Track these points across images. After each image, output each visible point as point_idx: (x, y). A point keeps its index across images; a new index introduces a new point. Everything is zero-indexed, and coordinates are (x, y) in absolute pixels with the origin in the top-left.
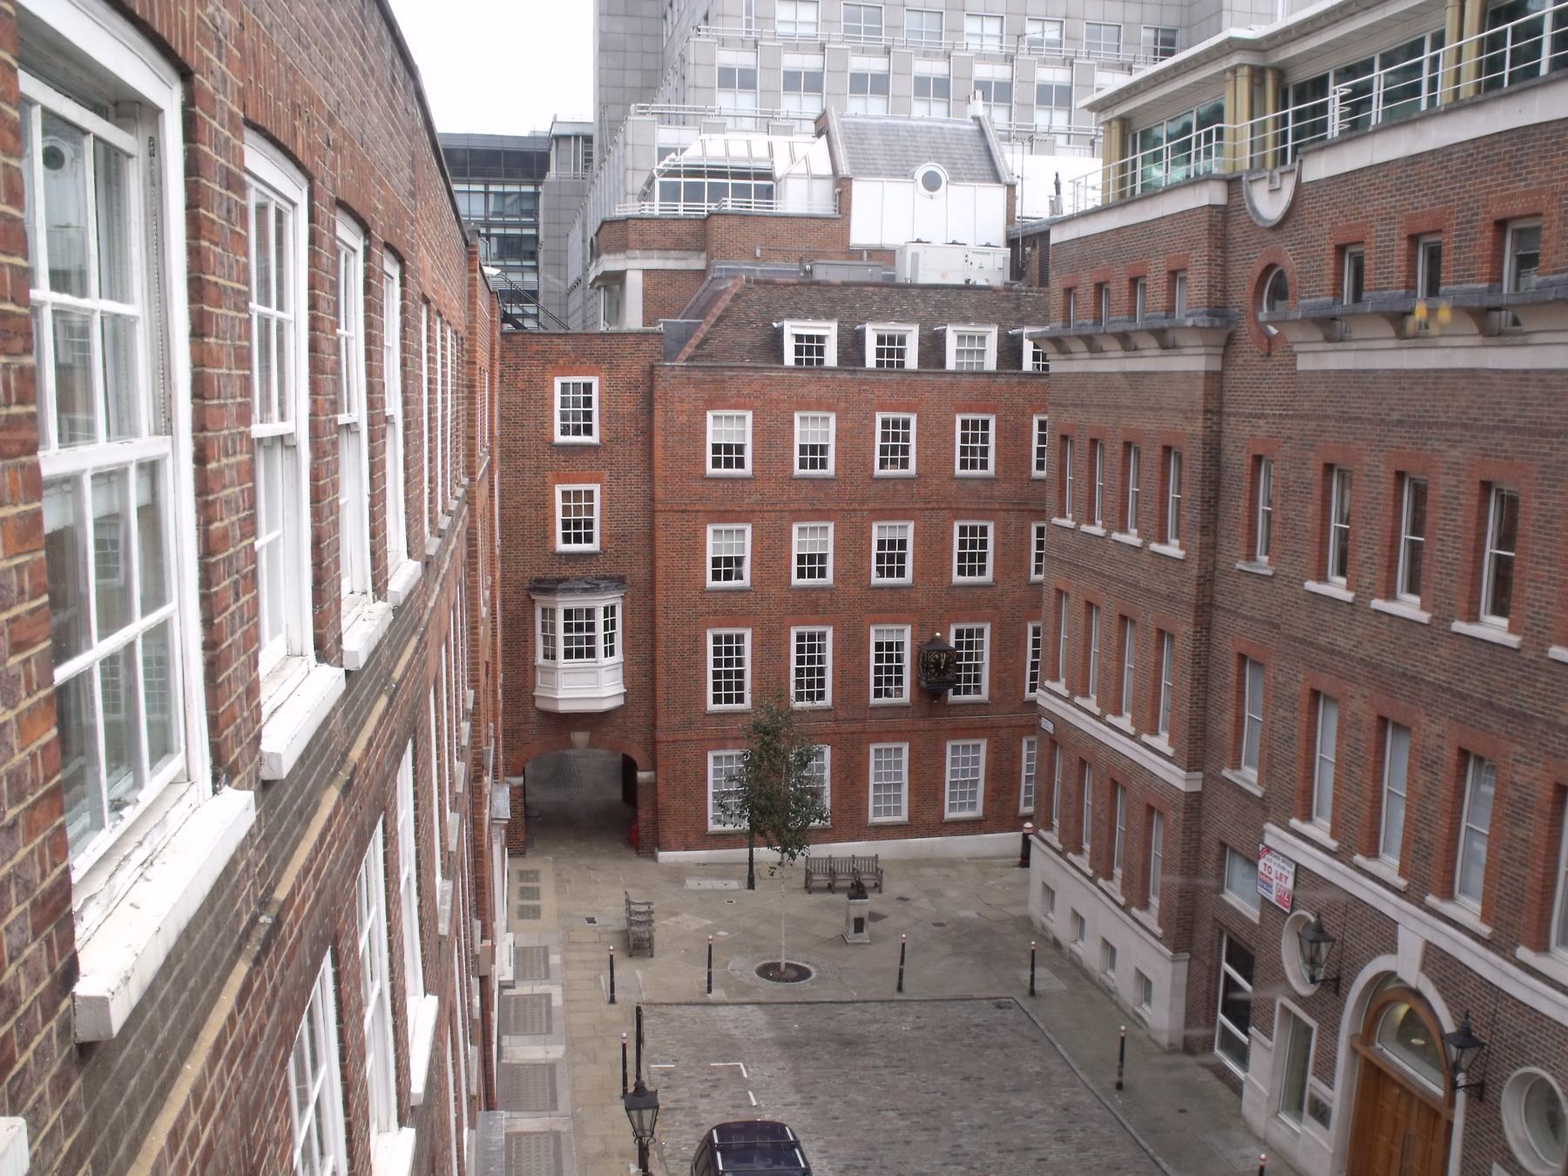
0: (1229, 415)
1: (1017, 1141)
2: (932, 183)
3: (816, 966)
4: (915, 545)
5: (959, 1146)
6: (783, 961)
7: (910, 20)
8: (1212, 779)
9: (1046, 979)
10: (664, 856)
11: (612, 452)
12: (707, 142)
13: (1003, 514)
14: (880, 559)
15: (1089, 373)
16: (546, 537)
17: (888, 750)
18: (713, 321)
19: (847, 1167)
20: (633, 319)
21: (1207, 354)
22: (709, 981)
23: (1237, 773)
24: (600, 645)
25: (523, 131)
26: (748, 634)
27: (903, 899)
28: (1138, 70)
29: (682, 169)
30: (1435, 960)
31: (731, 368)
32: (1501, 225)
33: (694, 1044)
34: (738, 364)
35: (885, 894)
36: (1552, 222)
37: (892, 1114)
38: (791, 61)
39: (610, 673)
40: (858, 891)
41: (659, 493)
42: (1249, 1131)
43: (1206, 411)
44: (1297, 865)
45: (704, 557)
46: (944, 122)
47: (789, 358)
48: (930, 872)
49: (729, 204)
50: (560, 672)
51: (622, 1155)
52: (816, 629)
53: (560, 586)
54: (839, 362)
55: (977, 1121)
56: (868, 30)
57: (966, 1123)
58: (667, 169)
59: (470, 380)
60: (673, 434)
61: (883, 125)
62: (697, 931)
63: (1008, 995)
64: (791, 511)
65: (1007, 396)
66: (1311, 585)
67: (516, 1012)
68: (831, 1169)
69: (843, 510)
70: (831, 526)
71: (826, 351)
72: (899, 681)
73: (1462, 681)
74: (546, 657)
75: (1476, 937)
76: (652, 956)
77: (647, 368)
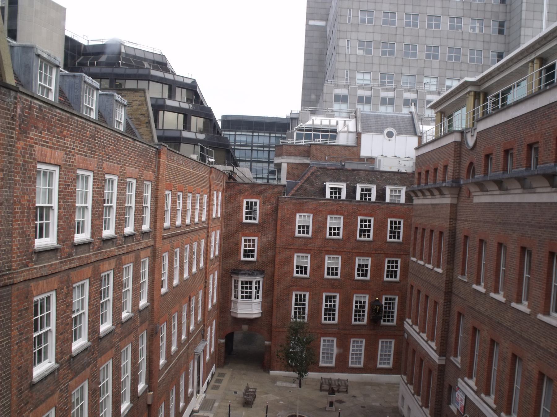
0: (459, 220)
2: (390, 135)
4: (371, 266)
7: (403, 79)
8: (448, 360)
10: (272, 372)
11: (262, 226)
13: (404, 256)
14: (359, 270)
18: (303, 181)
20: (284, 181)
23: (456, 359)
24: (253, 295)
25: (284, 116)
26: (307, 294)
27: (354, 397)
28: (442, 94)
29: (304, 129)
31: (306, 199)
32: (530, 146)
34: (310, 197)
35: (349, 394)
36: (542, 145)
38: (361, 93)
39: (256, 305)
40: (332, 392)
41: (278, 242)
43: (450, 219)
44: (466, 396)
46: (370, 112)
47: (328, 196)
48: (369, 387)
49: (317, 141)
50: (239, 303)
52: (333, 294)
56: (388, 82)
59: (156, 195)
61: (376, 115)
62: (272, 401)
65: (408, 212)
66: (474, 286)
69: (345, 252)
70: (340, 258)
71: (372, 195)
72: (363, 315)
73: (514, 326)
74: (235, 297)
76: (251, 407)
77: (277, 198)
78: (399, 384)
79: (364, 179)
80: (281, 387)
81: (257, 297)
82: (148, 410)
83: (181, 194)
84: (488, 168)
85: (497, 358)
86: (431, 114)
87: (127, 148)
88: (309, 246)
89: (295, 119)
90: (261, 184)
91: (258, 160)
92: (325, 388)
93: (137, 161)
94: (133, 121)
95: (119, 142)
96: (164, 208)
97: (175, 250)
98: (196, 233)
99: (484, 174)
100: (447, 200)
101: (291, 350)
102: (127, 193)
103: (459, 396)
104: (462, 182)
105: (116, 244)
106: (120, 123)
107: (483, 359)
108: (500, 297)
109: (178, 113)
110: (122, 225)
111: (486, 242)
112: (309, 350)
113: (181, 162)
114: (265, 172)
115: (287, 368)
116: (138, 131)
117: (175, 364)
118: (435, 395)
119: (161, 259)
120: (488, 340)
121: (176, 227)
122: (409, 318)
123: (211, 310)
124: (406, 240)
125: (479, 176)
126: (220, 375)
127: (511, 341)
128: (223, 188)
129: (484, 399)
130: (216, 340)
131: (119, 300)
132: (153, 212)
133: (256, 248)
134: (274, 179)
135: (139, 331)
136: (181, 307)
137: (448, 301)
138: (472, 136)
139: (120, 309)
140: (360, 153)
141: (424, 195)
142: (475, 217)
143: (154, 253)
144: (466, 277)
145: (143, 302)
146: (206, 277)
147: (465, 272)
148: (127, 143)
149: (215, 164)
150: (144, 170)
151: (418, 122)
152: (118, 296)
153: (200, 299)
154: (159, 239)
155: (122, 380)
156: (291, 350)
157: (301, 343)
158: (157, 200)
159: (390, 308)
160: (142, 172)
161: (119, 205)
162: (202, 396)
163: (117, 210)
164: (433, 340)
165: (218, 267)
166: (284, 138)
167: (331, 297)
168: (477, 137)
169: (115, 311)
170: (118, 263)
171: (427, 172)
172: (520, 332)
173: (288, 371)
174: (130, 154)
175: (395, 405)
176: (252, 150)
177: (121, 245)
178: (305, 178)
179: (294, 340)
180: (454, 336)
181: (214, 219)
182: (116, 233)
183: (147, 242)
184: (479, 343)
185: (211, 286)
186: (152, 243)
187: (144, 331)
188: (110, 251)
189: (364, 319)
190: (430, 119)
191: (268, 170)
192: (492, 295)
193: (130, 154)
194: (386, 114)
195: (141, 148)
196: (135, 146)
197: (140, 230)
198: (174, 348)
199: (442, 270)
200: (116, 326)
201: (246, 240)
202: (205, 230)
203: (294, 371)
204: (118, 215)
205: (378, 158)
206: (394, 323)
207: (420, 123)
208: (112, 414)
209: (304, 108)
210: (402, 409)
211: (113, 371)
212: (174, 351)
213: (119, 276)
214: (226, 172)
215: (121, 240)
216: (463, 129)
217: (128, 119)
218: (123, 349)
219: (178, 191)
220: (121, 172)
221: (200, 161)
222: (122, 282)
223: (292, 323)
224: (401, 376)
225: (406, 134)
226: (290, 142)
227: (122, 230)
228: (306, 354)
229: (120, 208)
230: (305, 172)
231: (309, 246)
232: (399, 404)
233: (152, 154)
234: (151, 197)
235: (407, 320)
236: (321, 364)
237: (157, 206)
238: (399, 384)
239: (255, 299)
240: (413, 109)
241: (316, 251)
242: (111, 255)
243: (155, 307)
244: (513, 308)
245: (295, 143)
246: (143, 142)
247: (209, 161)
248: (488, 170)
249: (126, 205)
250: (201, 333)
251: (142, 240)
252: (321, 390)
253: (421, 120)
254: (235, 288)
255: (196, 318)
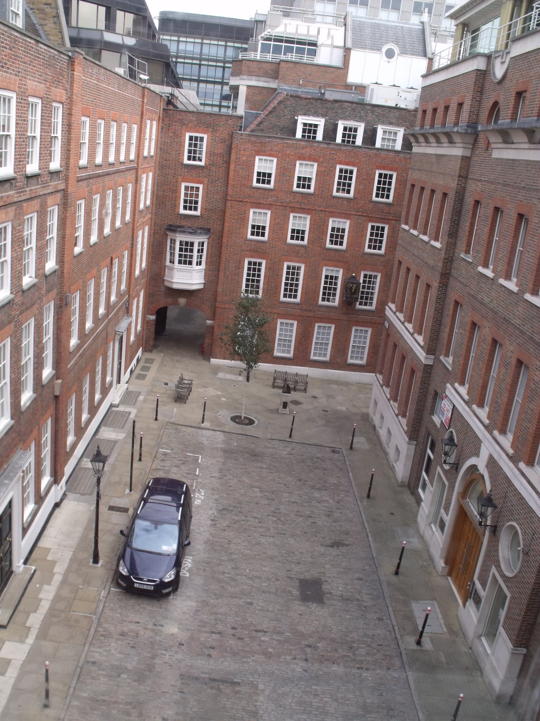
1: (308, 512)
2: (390, 54)
3: (258, 420)
5: (279, 509)
6: (243, 415)
8: (437, 360)
9: (360, 442)
10: (213, 361)
12: (288, 25)
13: (393, 222)
14: (332, 236)
15: (425, 154)
16: (175, 206)
17: (324, 327)
18: (267, 113)
19: (224, 509)
20: (241, 111)
21: (464, 147)
22: (203, 418)
23: (446, 359)
24: (195, 260)
26: (264, 262)
27: (315, 397)
29: (273, 37)
30: (492, 463)
31: (269, 137)
33: (184, 444)
34: (275, 135)
35: (308, 394)
37: (257, 490)
40: (287, 390)
41: (230, 191)
42: (418, 530)
43: (460, 176)
44: (454, 406)
45: (248, 224)
47: (299, 134)
48: (335, 386)
49: (290, 57)
50: (175, 270)
51: (125, 485)
53: (178, 229)
54: (323, 139)
55: (293, 500)
57: (287, 499)
58: (265, 37)
59: (69, 123)
60: (239, 165)
61: (373, 23)
62: (212, 396)
63: (340, 447)
64: (289, 207)
65: (403, 163)
66: (480, 269)
67: (113, 417)
68: (216, 509)
71: (357, 137)
72: (334, 295)
74: (171, 262)
75: (507, 455)
76: (185, 403)
78: (372, 385)
79: (349, 114)
80: (224, 379)
81: (199, 263)
82: (54, 403)
83: (103, 122)
84: (518, 111)
85: (498, 363)
86: (450, 25)
87: (28, 53)
88: (270, 199)
89: (262, 22)
90: (210, 114)
91: (208, 79)
92: (279, 385)
93: (42, 72)
94: (35, 12)
95: (17, 45)
96: (79, 140)
97: (94, 197)
98: (122, 174)
99: (511, 118)
100: (457, 151)
101: (239, 333)
102: (30, 117)
103: (445, 405)
104: (480, 128)
105: (16, 186)
106: (17, 14)
107: (480, 363)
108: (512, 285)
109: (98, 5)
110: (23, 161)
111: (502, 211)
112: (262, 334)
113: (102, 78)
114: (217, 96)
115: (234, 355)
116: (43, 28)
117: (90, 345)
118: (415, 403)
119: (75, 208)
120: (489, 340)
121: (96, 166)
122: (393, 302)
123: (138, 278)
124: (397, 201)
125: (504, 121)
126: (147, 361)
127: (517, 344)
128: (159, 117)
129: (476, 411)
130: (144, 317)
131: (20, 261)
132: (65, 144)
133: (200, 200)
134: (228, 107)
135: (44, 301)
136: (99, 271)
137: (444, 284)
138: (503, 63)
139: (20, 272)
140: (347, 77)
141: (427, 141)
142: (492, 177)
143: (65, 199)
144: (470, 256)
145: (51, 265)
146: (133, 233)
147: (470, 249)
148: (28, 46)
149: (148, 83)
150: (52, 86)
151: (430, 37)
152: (17, 256)
153: (125, 262)
154: (72, 181)
155: (22, 364)
156: (239, 333)
157: (252, 324)
158: (71, 129)
159: (369, 288)
160: (50, 89)
161: (19, 135)
162: (123, 386)
163: (16, 141)
164: (420, 333)
165: (149, 222)
166: (245, 50)
167: (294, 268)
168: (509, 65)
169: (15, 275)
170: (17, 212)
171: (435, 110)
172: (530, 333)
173: (233, 360)
174: (32, 62)
175: (365, 410)
176: (200, 65)
177: (22, 188)
178: (269, 109)
179: (244, 320)
180: (447, 330)
181: (145, 158)
182: (15, 172)
183: (56, 185)
184: (477, 341)
185: (139, 246)
186: (62, 187)
187: (51, 301)
188: (8, 197)
189: (334, 299)
190: (447, 34)
191: (221, 94)
192: (502, 281)
193: (32, 62)
194: (389, 24)
195: (47, 54)
196: (38, 50)
197: (47, 168)
198: (89, 325)
199: (441, 244)
200: (15, 294)
201: (187, 188)
202: (133, 172)
203: (241, 360)
204: (18, 148)
205: (371, 87)
206: (373, 307)
207: (433, 39)
208: (11, 405)
209: (275, 7)
210: (373, 416)
211: (11, 352)
212: (89, 328)
213: (19, 229)
214: (163, 95)
215: (22, 182)
216: (492, 52)
217: (28, 10)
218: (24, 324)
219: (99, 118)
220: (21, 88)
221: (128, 78)
222: (23, 237)
223: (243, 298)
224: (376, 375)
225: (412, 54)
226: (251, 55)
227: (23, 168)
228: (257, 339)
229: (20, 138)
230: (270, 100)
231: (270, 199)
232: (370, 411)
233: (63, 64)
234: (62, 125)
235: (390, 304)
236: (276, 354)
237: (70, 137)
238: (372, 385)
239: (197, 265)
240: (425, 17)
241: (278, 207)
242: (8, 201)
243: (65, 271)
244: (527, 300)
245: (258, 58)
246: (50, 45)
247: (140, 78)
248: (517, 114)
249: (29, 134)
250: (125, 306)
251: (51, 182)
252: (274, 387)
253: (435, 34)
254: (171, 249)
255: (119, 286)
